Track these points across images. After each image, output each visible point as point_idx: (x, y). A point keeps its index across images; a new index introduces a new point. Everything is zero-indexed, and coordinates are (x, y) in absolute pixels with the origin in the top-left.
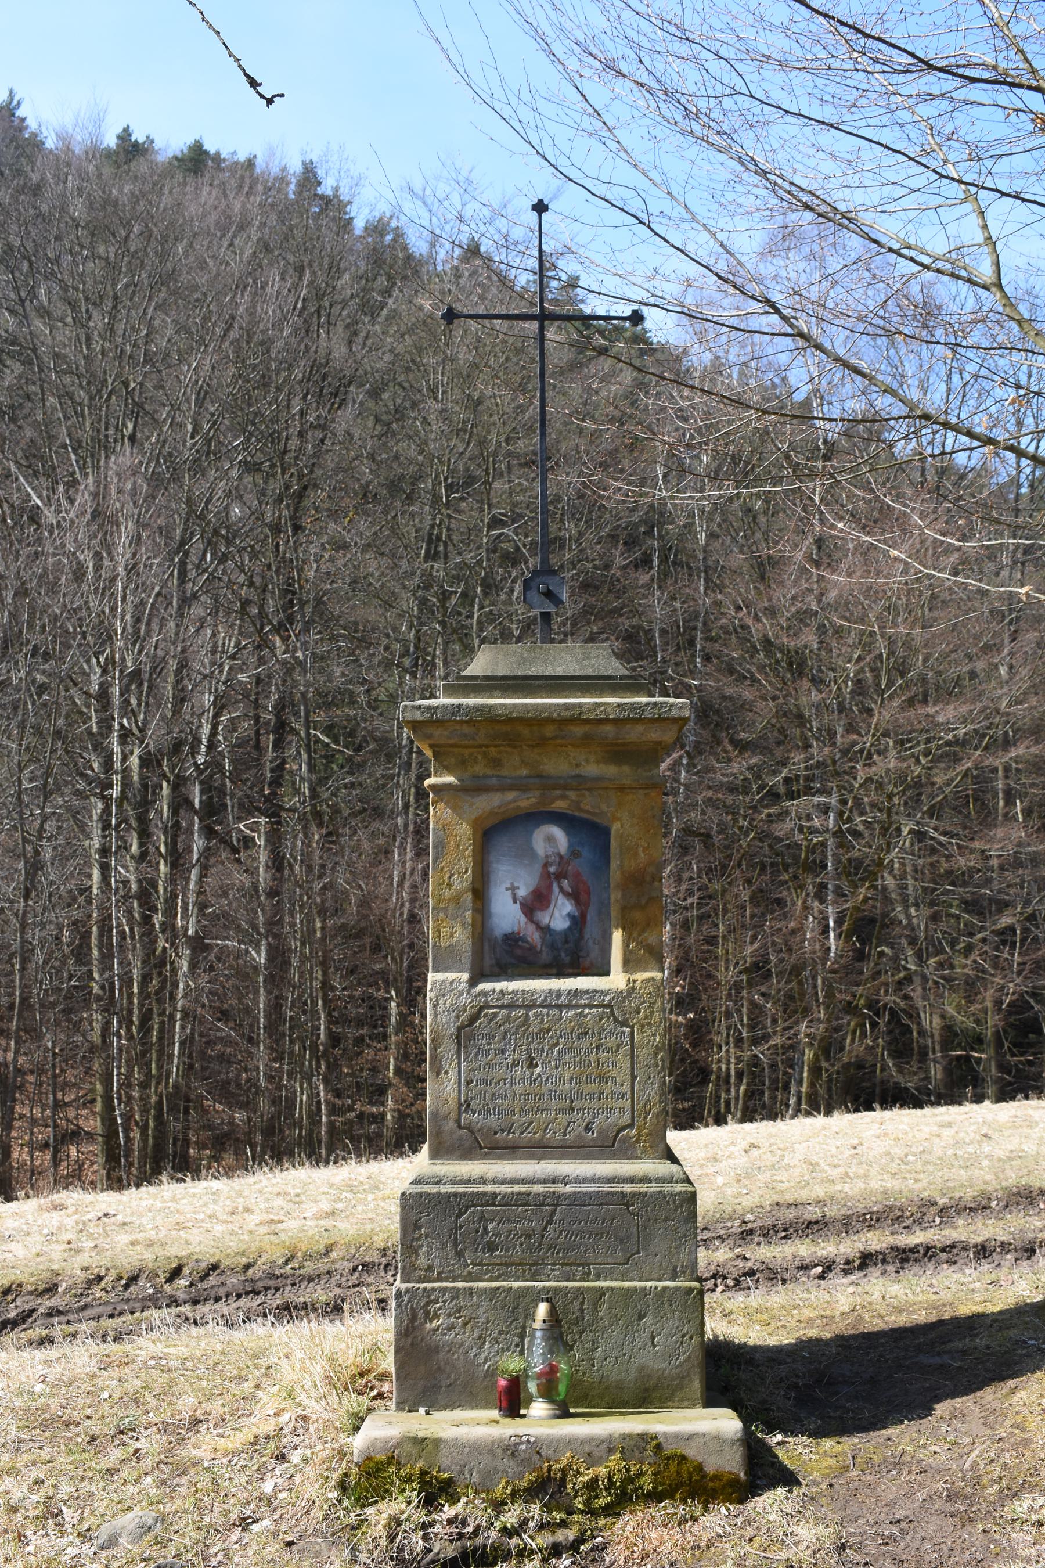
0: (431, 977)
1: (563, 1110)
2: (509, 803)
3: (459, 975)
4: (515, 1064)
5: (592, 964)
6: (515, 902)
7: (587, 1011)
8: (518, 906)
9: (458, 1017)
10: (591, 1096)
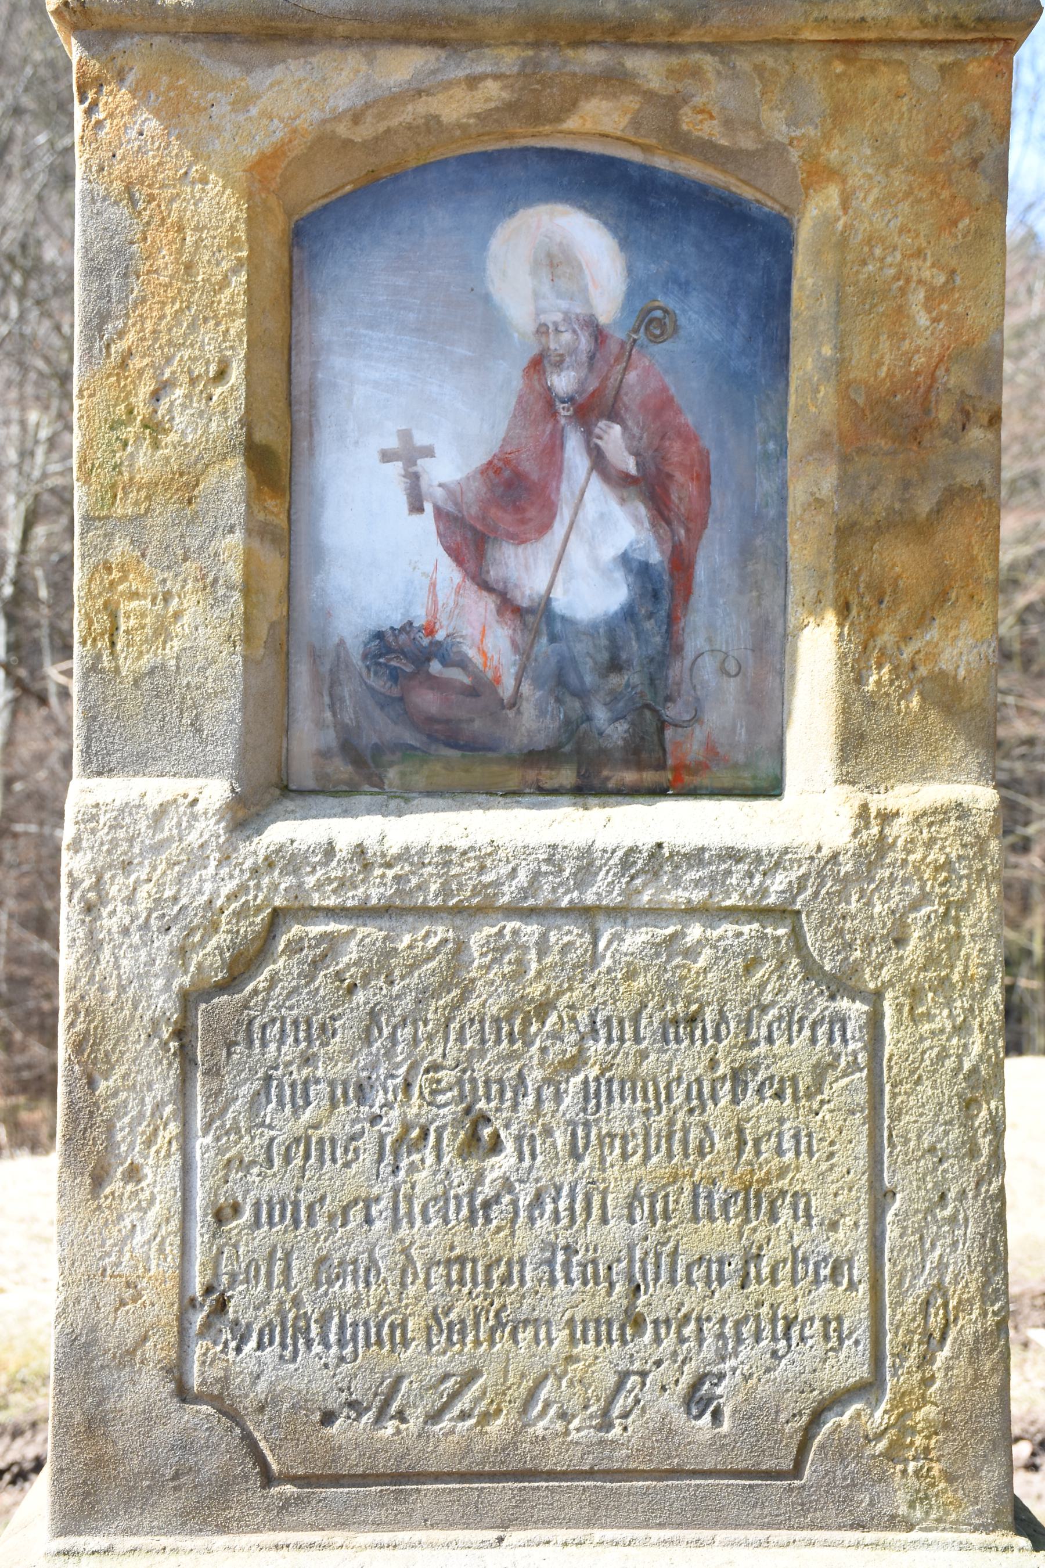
0: (82, 792)
1: (599, 1328)
2: (396, 99)
3: (190, 786)
4: (412, 1138)
5: (711, 748)
6: (416, 507)
7: (695, 932)
8: (427, 520)
9: (182, 952)
10: (712, 1270)
